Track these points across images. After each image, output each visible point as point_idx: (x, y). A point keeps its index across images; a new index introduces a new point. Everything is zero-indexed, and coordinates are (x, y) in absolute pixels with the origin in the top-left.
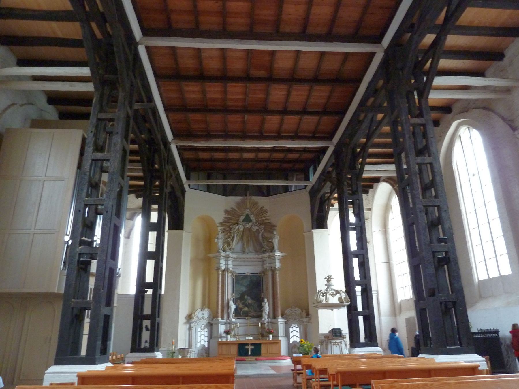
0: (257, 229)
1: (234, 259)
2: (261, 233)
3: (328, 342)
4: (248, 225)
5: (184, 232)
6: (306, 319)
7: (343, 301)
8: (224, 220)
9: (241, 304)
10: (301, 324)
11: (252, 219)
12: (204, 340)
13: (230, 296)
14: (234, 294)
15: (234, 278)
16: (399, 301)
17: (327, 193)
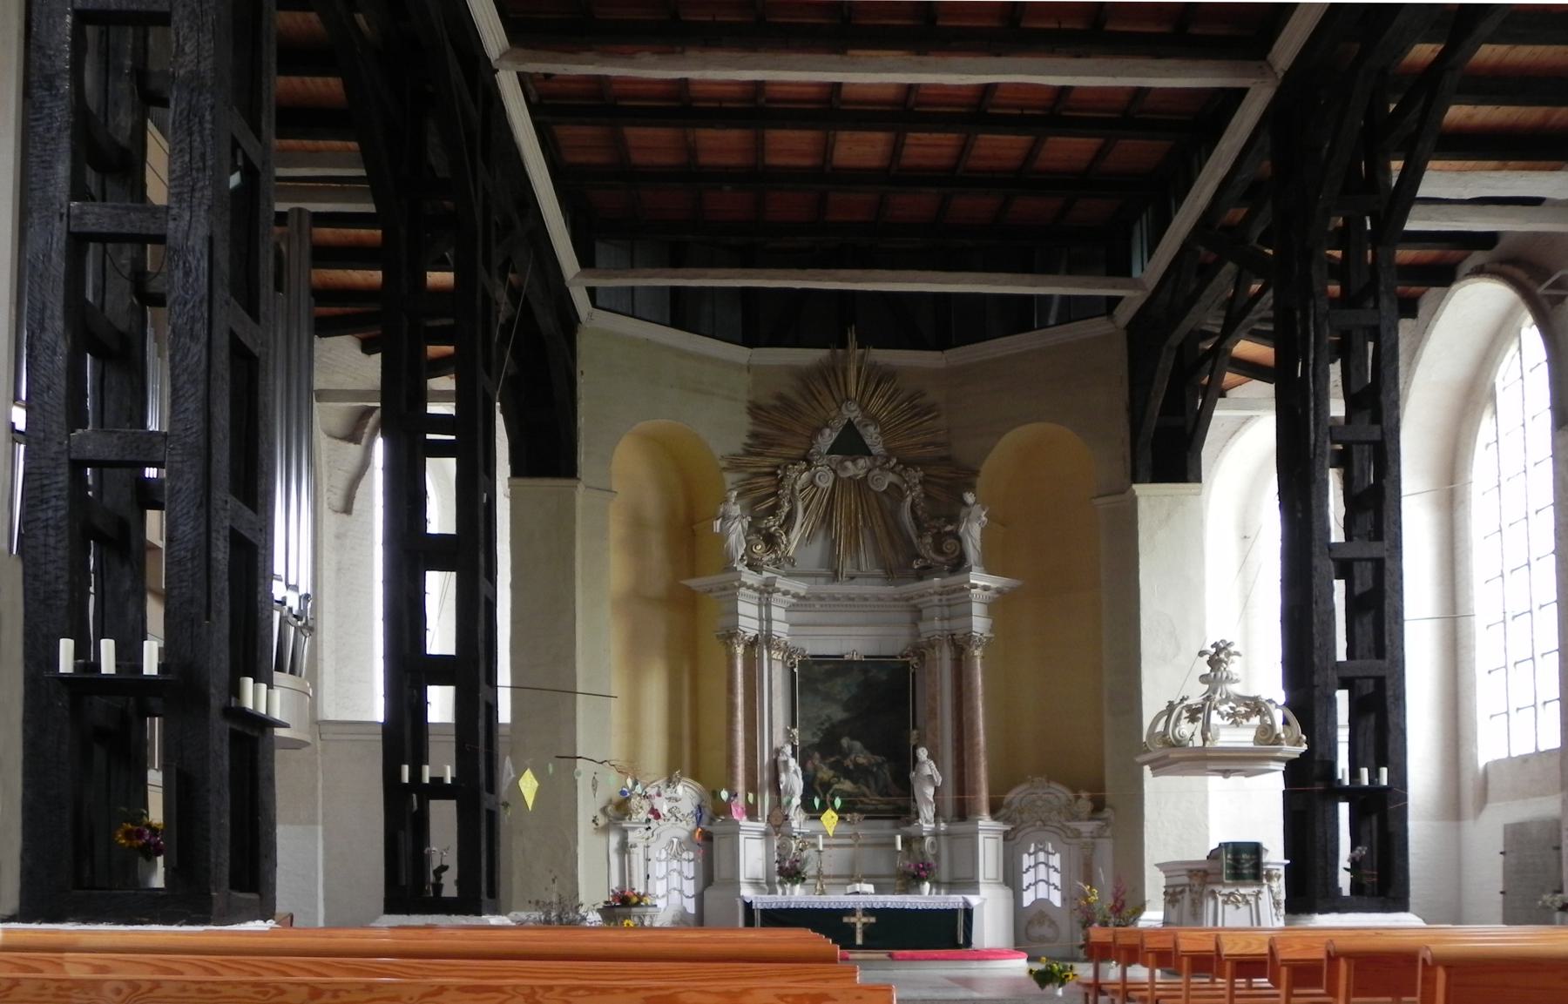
0: (891, 484)
1: (794, 601)
2: (909, 499)
3: (1201, 894)
4: (856, 468)
5: (581, 487)
6: (1090, 823)
7: (1281, 739)
8: (745, 444)
9: (825, 769)
10: (1069, 841)
11: (868, 441)
12: (681, 891)
13: (779, 739)
14: (796, 731)
15: (796, 670)
16: (1481, 765)
17: (1206, 335)
